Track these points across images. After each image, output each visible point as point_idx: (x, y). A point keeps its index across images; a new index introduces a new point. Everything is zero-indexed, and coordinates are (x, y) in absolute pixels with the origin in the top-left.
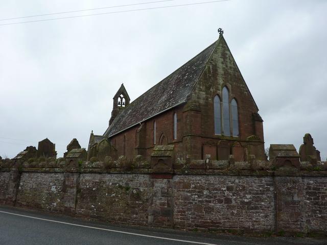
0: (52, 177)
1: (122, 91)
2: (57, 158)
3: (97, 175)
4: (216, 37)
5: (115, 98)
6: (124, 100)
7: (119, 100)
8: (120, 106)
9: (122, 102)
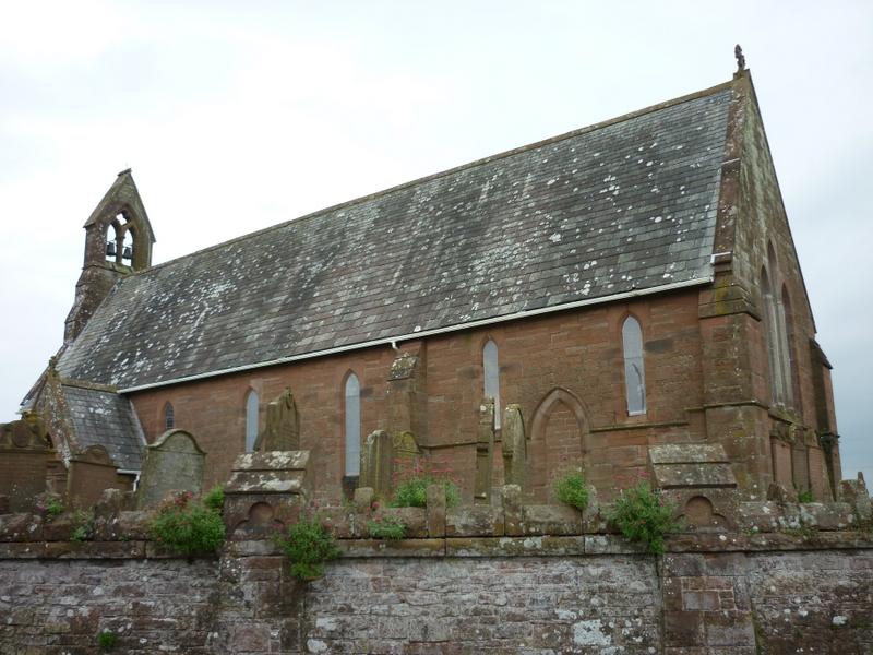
0: (559, 579)
1: (122, 207)
2: (153, 265)
3: (833, 557)
4: (725, 72)
5: (94, 227)
6: (128, 241)
7: (111, 234)
8: (113, 259)
9: (120, 246)
